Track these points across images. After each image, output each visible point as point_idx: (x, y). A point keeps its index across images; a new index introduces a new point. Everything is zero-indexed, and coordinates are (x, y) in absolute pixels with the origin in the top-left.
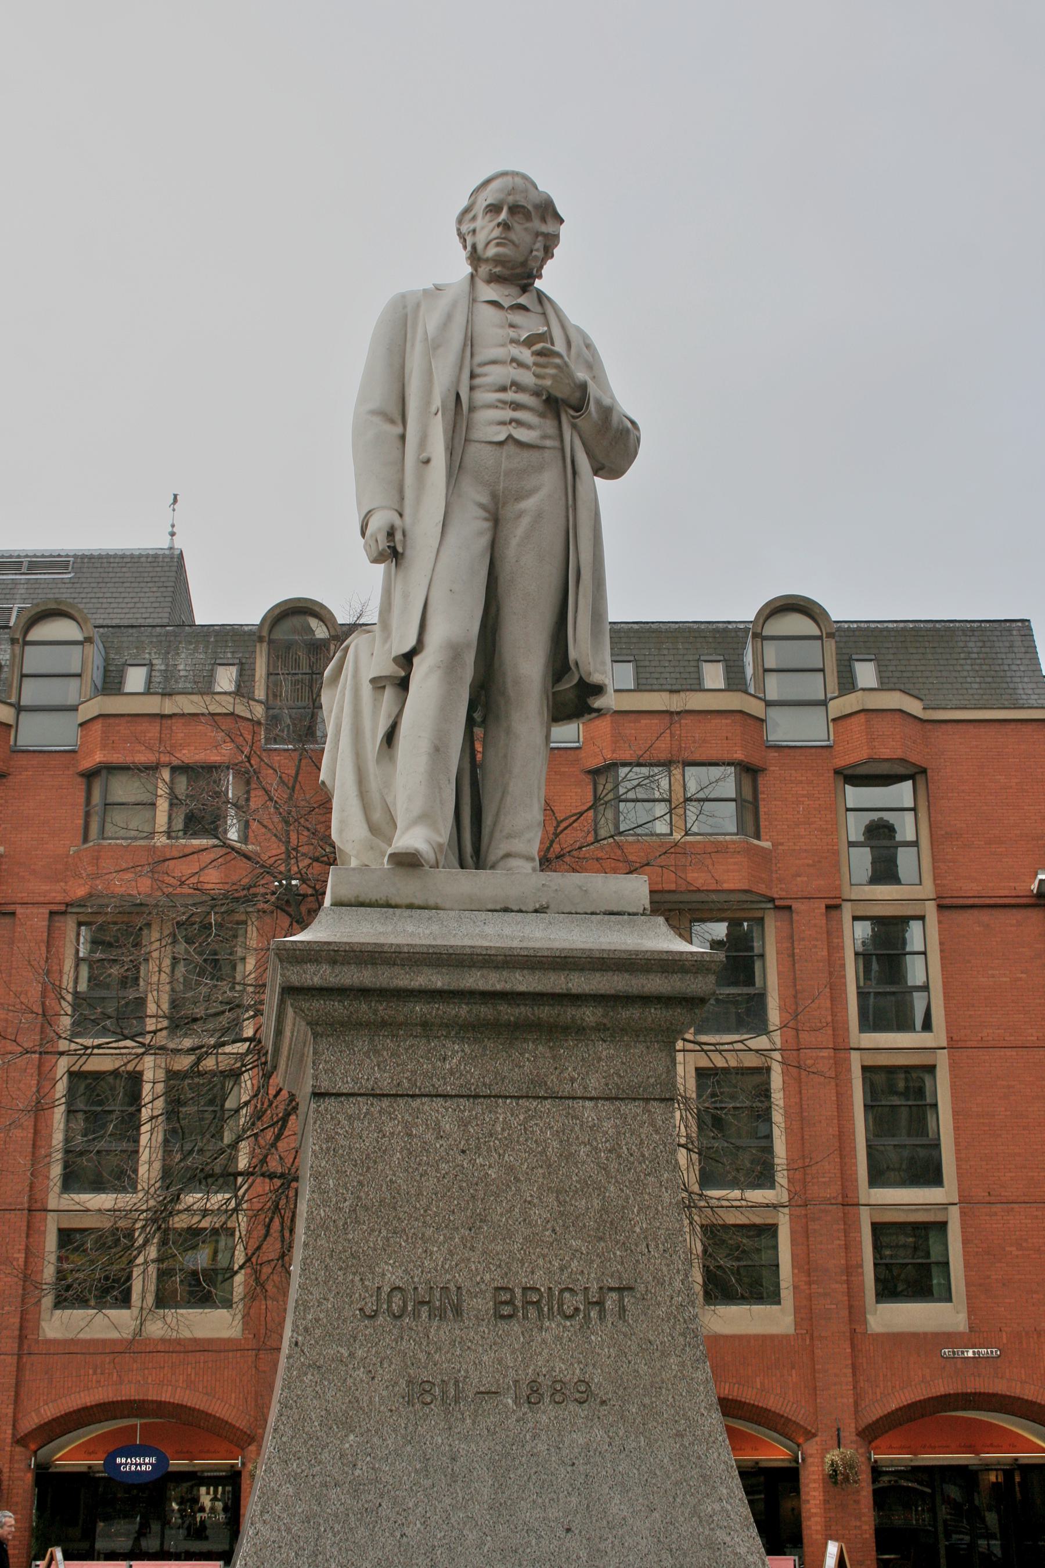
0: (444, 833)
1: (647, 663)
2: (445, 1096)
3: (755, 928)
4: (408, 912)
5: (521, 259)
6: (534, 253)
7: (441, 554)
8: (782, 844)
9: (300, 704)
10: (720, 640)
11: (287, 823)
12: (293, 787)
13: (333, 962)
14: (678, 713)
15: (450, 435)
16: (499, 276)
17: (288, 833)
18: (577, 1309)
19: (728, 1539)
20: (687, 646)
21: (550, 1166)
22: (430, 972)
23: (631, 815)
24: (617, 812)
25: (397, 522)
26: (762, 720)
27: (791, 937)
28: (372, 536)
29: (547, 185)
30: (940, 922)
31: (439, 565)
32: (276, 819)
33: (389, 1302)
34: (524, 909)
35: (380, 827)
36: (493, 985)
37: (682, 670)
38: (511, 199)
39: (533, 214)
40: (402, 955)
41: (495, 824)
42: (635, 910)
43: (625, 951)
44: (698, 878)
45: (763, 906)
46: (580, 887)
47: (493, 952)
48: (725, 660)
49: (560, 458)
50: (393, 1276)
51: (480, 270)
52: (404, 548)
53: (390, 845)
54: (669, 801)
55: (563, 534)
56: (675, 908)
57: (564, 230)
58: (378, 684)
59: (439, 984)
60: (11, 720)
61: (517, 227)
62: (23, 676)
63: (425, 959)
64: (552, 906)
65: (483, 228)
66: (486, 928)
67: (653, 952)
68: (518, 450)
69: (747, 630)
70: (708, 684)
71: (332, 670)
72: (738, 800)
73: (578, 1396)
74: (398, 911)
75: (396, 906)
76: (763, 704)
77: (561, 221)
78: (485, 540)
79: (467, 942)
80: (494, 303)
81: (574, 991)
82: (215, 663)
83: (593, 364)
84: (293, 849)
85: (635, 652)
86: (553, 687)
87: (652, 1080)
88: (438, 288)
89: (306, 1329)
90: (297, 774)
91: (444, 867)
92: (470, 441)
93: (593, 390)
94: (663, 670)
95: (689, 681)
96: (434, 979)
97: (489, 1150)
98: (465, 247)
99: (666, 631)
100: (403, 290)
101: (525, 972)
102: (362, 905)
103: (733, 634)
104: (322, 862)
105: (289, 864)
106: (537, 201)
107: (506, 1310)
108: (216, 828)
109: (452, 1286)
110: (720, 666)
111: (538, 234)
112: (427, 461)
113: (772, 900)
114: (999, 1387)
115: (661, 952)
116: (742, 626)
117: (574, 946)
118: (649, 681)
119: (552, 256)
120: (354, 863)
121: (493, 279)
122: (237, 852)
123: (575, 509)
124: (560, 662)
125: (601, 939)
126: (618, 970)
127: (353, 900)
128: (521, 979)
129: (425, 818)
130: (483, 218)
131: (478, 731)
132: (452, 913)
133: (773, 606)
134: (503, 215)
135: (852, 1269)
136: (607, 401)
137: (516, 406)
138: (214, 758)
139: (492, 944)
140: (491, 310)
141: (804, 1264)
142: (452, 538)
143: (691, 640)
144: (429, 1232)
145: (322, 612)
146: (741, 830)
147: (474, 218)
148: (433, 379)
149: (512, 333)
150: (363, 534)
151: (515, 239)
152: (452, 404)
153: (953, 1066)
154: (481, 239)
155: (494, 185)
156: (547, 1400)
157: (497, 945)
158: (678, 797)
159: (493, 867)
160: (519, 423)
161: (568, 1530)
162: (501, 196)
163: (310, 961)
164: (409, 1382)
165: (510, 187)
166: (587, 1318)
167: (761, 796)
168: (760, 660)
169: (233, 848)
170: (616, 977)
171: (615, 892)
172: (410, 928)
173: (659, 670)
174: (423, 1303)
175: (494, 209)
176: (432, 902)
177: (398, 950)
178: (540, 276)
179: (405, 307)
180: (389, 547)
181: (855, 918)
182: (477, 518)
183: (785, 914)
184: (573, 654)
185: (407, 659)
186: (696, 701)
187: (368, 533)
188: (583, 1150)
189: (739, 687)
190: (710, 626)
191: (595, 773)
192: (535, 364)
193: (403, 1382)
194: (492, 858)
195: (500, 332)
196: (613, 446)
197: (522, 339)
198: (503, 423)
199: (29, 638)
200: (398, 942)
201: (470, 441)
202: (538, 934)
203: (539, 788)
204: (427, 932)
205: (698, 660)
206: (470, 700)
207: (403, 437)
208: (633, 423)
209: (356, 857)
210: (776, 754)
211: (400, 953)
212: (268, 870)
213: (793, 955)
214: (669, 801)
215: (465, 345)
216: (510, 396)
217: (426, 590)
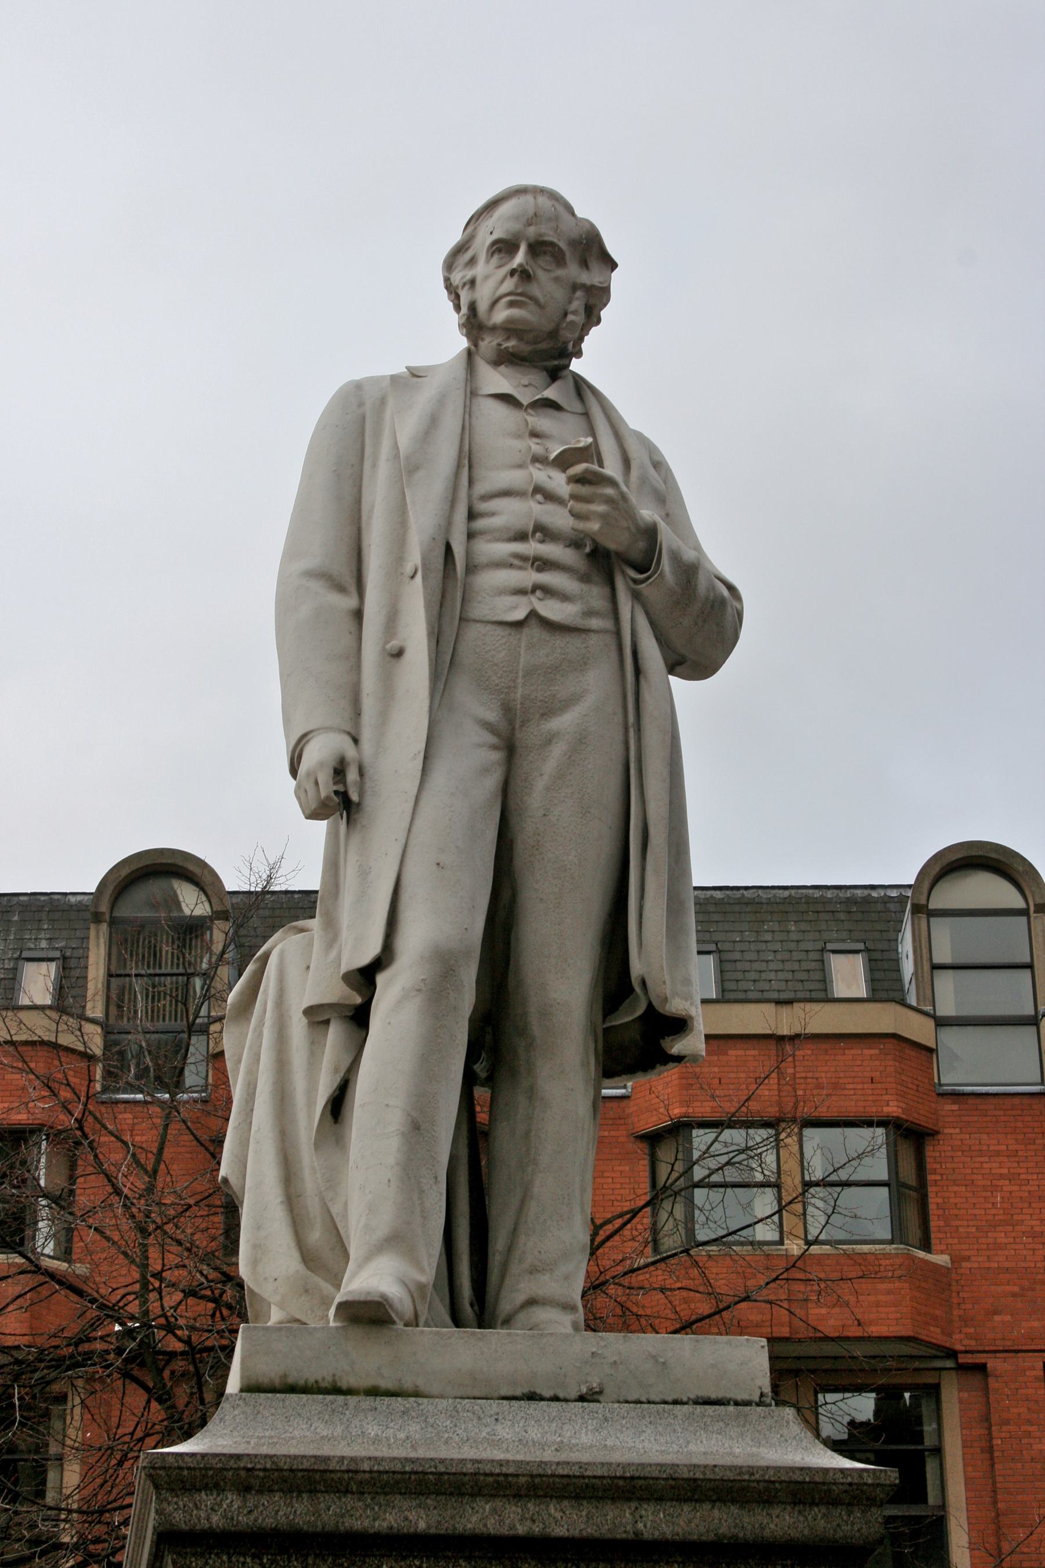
0: (427, 1267)
1: (737, 956)
3: (924, 1402)
4: (368, 1402)
5: (548, 327)
6: (570, 317)
7: (423, 803)
8: (967, 1259)
9: (160, 1025)
10: (859, 916)
11: (144, 1231)
12: (155, 1171)
13: (245, 1489)
14: (794, 1038)
15: (435, 612)
16: (513, 355)
17: (144, 1247)
20: (803, 926)
22: (406, 1504)
23: (715, 1213)
24: (690, 1202)
25: (351, 752)
26: (930, 1050)
27: (986, 1418)
28: (308, 774)
31: (418, 822)
32: (126, 1224)
34: (561, 1396)
35: (322, 1255)
36: (512, 1527)
37: (796, 966)
38: (532, 231)
39: (568, 255)
40: (359, 1477)
41: (510, 1249)
42: (745, 1397)
43: (731, 1468)
44: (830, 1319)
45: (938, 1364)
46: (655, 1358)
47: (511, 1470)
48: (867, 950)
49: (613, 647)
51: (483, 344)
52: (361, 793)
53: (338, 1287)
54: (777, 1186)
55: (619, 768)
56: (801, 1374)
58: (318, 1016)
59: (422, 1525)
63: (397, 1482)
64: (607, 1391)
65: (486, 278)
66: (499, 1428)
67: (778, 1469)
68: (545, 635)
69: (902, 900)
70: (840, 990)
71: (241, 993)
72: (894, 1184)
74: (352, 1400)
75: (349, 1392)
76: (931, 1023)
78: (492, 782)
79: (468, 1453)
80: (505, 398)
82: (19, 958)
83: (666, 495)
84: (154, 1276)
85: (717, 937)
86: (604, 1022)
88: (414, 373)
90: (161, 1150)
91: (427, 1324)
92: (468, 620)
93: (667, 536)
94: (763, 966)
95: (809, 986)
96: (412, 1516)
98: (458, 308)
99: (769, 902)
100: (358, 375)
101: (565, 1503)
102: (292, 1389)
103: (880, 907)
104: (202, 1297)
105: (146, 1301)
106: (574, 234)
108: (22, 1243)
110: (859, 960)
111: (575, 287)
112: (399, 654)
113: (952, 1354)
115: (792, 1469)
116: (894, 893)
117: (645, 1460)
118: (743, 985)
119: (598, 321)
120: (276, 1315)
121: (504, 359)
122: (60, 1282)
123: (639, 730)
124: (615, 981)
125: (692, 1447)
126: (719, 1500)
127: (277, 1381)
128: (558, 1515)
129: (396, 1241)
130: (488, 261)
131: (481, 1093)
132: (443, 1404)
133: (945, 861)
134: (520, 257)
136: (689, 555)
137: (543, 564)
138: (21, 1117)
139: (509, 1457)
140: (500, 410)
142: (439, 778)
143: (811, 916)
145: (207, 879)
146: (899, 1235)
147: (472, 262)
148: (406, 523)
149: (535, 447)
150: (294, 772)
151: (538, 289)
152: (438, 562)
154: (484, 295)
155: (505, 209)
157: (519, 1457)
158: (792, 1184)
159: (507, 1322)
160: (547, 591)
162: (516, 227)
163: (206, 1487)
165: (531, 212)
167: (929, 1177)
168: (925, 951)
169: (52, 1275)
170: (716, 1512)
171: (713, 1366)
172: (373, 1430)
173: (756, 966)
175: (504, 247)
176: (408, 1385)
177: (353, 1467)
178: (579, 354)
179: (361, 404)
180: (336, 793)
182: (480, 745)
183: (975, 1379)
184: (637, 967)
185: (366, 978)
186: (821, 1019)
187: (303, 769)
189: (892, 995)
190: (841, 894)
191: (653, 1139)
192: (574, 497)
194: (505, 1306)
195: (518, 444)
196: (702, 627)
197: (552, 456)
198: (521, 592)
200: (352, 1454)
201: (468, 620)
202: (586, 1438)
203: (583, 1190)
204: (402, 1435)
205: (823, 950)
206: (469, 1041)
207: (358, 615)
208: (731, 588)
209: (281, 1306)
210: (955, 1107)
211: (356, 1472)
212: (112, 1312)
213: (990, 1449)
214: (777, 1186)
215: (459, 467)
216: (533, 547)
217: (398, 862)
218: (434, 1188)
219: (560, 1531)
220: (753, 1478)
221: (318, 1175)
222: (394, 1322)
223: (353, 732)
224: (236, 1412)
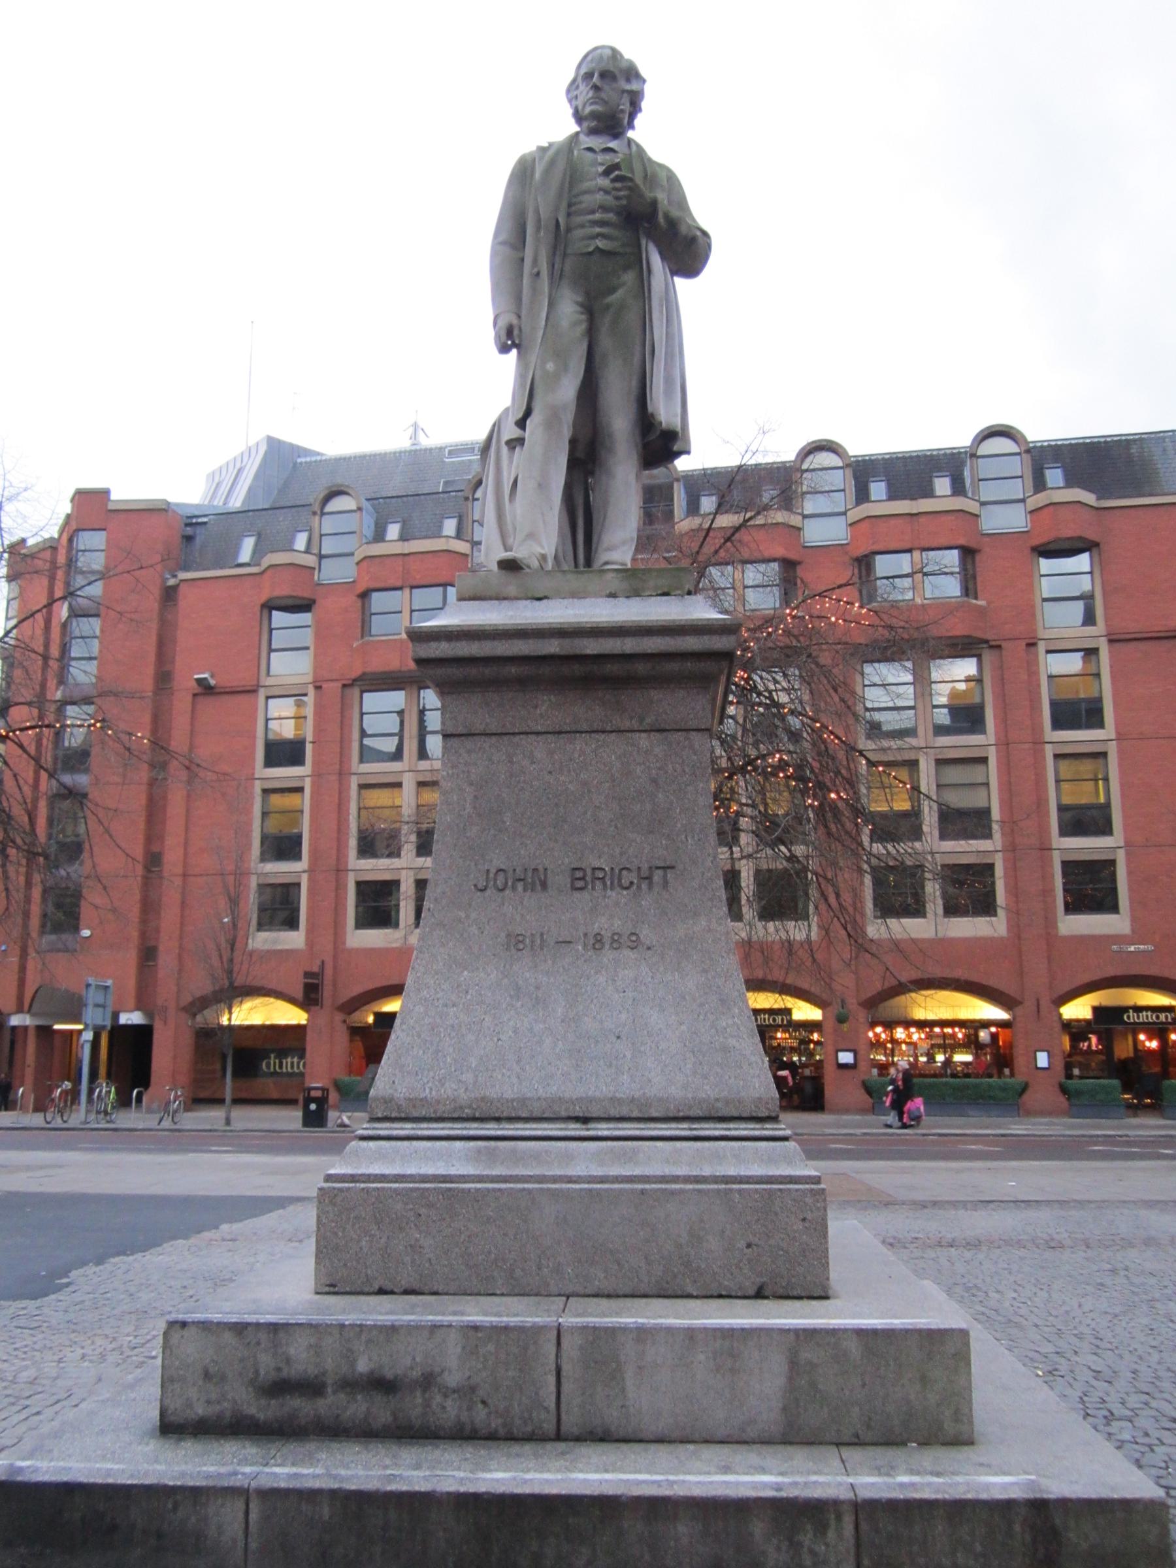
2: (538, 733)
18: (632, 883)
19: (737, 1045)
21: (614, 781)
26: (977, 516)
27: (1001, 667)
29: (629, 53)
30: (1110, 652)
33: (495, 880)
50: (498, 862)
57: (647, 89)
60: (468, 552)
61: (606, 87)
69: (966, 452)
70: (938, 493)
73: (630, 944)
76: (978, 504)
77: (644, 81)
81: (628, 652)
87: (692, 716)
89: (436, 900)
97: (569, 771)
107: (580, 884)
109: (541, 868)
111: (624, 91)
113: (987, 642)
114: (1154, 971)
119: (640, 110)
135: (1048, 892)
141: (1014, 891)
144: (525, 831)
151: (609, 93)
153: (1120, 751)
155: (589, 58)
156: (607, 946)
161: (618, 1037)
164: (508, 935)
166: (639, 887)
174: (520, 880)
175: (589, 76)
181: (1048, 652)
183: (996, 652)
188: (639, 769)
193: (503, 935)
196: (688, 251)
207: (522, 260)
213: (1003, 679)
219: (588, 652)
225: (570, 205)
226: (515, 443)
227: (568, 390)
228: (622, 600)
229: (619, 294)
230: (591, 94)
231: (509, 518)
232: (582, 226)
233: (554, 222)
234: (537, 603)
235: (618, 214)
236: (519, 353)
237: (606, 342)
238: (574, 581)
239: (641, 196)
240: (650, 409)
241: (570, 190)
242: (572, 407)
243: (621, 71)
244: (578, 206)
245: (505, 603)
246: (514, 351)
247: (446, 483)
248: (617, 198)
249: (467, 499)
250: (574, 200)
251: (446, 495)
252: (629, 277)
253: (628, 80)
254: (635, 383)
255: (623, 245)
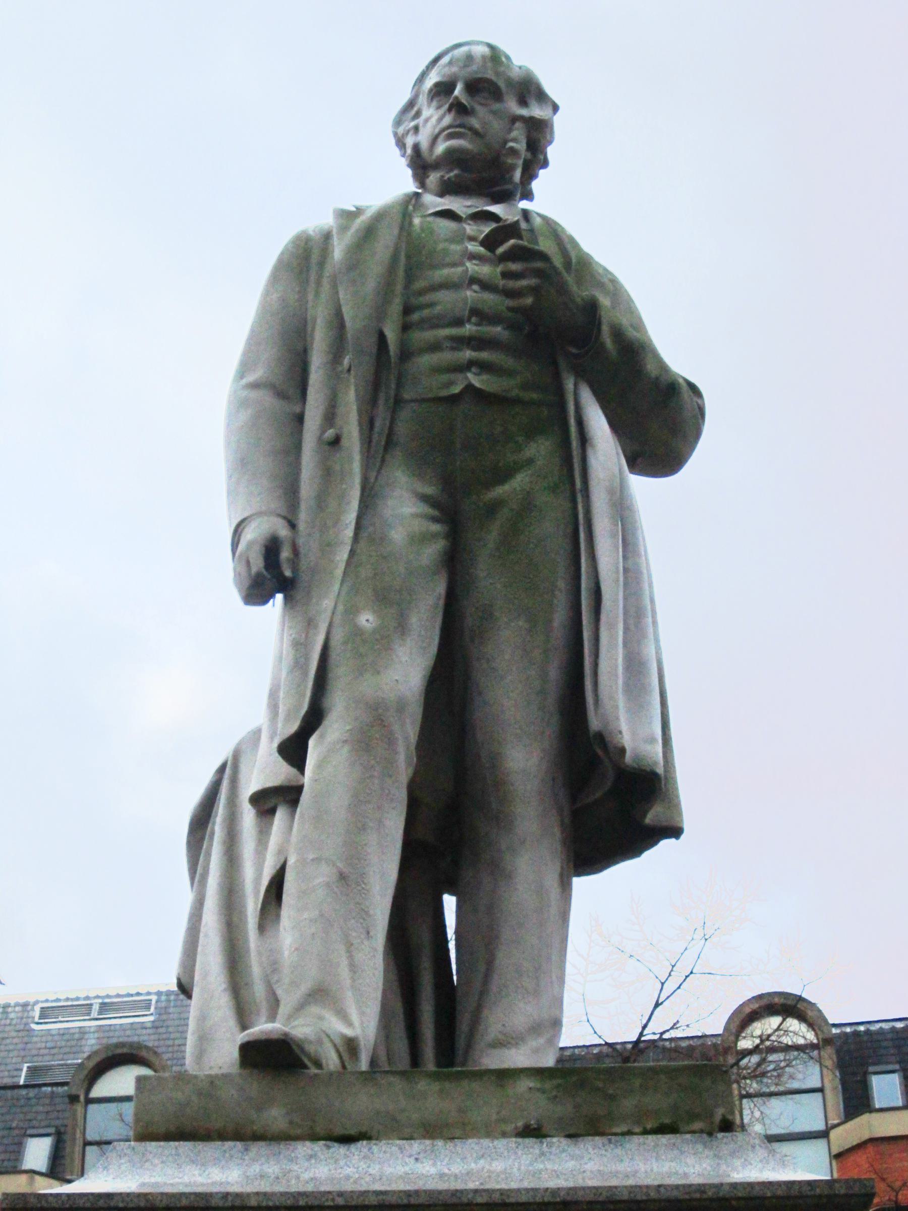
29: (522, 58)
57: (559, 122)
61: (481, 111)
62: (87, 1143)
111: (515, 119)
119: (545, 164)
151: (486, 128)
155: (445, 60)
175: (443, 89)
192: (506, 275)
196: (661, 421)
199: (96, 1092)
218: (366, 942)
220: (705, 1196)
221: (264, 959)
222: (305, 1067)
223: (290, 518)
224: (123, 1161)
225: (407, 310)
226: (276, 800)
227: (406, 671)
228: (558, 1142)
229: (519, 481)
230: (448, 120)
231: (256, 968)
232: (435, 347)
233: (374, 339)
234: (340, 1150)
235: (511, 326)
236: (288, 600)
237: (489, 580)
238: (432, 1096)
239: (562, 289)
240: (595, 724)
241: (410, 278)
242: (415, 711)
243: (510, 82)
244: (426, 312)
245: (258, 1149)
246: (279, 597)
247: (32, 1071)
248: (509, 294)
249: (74, 1099)
250: (414, 301)
251: (32, 1093)
252: (540, 450)
253: (523, 102)
254: (554, 672)
255: (525, 387)
